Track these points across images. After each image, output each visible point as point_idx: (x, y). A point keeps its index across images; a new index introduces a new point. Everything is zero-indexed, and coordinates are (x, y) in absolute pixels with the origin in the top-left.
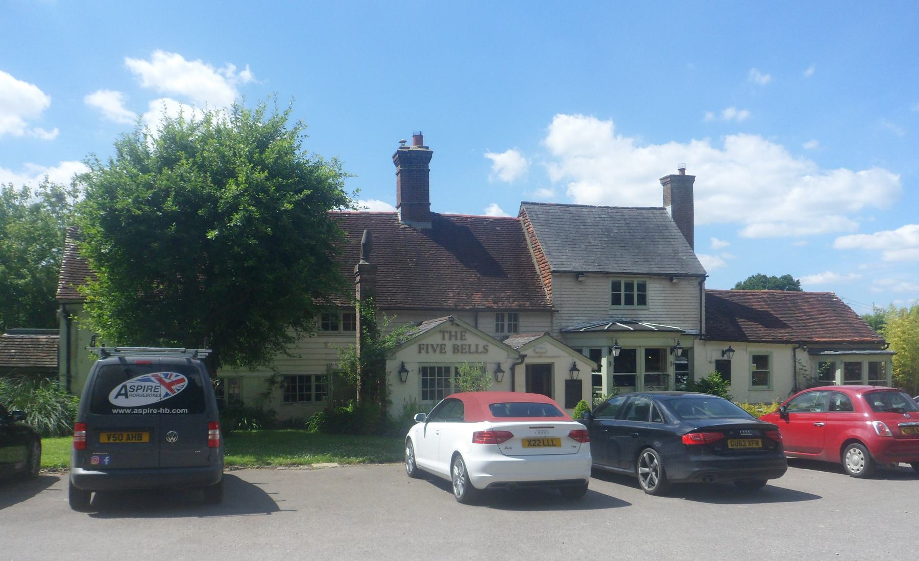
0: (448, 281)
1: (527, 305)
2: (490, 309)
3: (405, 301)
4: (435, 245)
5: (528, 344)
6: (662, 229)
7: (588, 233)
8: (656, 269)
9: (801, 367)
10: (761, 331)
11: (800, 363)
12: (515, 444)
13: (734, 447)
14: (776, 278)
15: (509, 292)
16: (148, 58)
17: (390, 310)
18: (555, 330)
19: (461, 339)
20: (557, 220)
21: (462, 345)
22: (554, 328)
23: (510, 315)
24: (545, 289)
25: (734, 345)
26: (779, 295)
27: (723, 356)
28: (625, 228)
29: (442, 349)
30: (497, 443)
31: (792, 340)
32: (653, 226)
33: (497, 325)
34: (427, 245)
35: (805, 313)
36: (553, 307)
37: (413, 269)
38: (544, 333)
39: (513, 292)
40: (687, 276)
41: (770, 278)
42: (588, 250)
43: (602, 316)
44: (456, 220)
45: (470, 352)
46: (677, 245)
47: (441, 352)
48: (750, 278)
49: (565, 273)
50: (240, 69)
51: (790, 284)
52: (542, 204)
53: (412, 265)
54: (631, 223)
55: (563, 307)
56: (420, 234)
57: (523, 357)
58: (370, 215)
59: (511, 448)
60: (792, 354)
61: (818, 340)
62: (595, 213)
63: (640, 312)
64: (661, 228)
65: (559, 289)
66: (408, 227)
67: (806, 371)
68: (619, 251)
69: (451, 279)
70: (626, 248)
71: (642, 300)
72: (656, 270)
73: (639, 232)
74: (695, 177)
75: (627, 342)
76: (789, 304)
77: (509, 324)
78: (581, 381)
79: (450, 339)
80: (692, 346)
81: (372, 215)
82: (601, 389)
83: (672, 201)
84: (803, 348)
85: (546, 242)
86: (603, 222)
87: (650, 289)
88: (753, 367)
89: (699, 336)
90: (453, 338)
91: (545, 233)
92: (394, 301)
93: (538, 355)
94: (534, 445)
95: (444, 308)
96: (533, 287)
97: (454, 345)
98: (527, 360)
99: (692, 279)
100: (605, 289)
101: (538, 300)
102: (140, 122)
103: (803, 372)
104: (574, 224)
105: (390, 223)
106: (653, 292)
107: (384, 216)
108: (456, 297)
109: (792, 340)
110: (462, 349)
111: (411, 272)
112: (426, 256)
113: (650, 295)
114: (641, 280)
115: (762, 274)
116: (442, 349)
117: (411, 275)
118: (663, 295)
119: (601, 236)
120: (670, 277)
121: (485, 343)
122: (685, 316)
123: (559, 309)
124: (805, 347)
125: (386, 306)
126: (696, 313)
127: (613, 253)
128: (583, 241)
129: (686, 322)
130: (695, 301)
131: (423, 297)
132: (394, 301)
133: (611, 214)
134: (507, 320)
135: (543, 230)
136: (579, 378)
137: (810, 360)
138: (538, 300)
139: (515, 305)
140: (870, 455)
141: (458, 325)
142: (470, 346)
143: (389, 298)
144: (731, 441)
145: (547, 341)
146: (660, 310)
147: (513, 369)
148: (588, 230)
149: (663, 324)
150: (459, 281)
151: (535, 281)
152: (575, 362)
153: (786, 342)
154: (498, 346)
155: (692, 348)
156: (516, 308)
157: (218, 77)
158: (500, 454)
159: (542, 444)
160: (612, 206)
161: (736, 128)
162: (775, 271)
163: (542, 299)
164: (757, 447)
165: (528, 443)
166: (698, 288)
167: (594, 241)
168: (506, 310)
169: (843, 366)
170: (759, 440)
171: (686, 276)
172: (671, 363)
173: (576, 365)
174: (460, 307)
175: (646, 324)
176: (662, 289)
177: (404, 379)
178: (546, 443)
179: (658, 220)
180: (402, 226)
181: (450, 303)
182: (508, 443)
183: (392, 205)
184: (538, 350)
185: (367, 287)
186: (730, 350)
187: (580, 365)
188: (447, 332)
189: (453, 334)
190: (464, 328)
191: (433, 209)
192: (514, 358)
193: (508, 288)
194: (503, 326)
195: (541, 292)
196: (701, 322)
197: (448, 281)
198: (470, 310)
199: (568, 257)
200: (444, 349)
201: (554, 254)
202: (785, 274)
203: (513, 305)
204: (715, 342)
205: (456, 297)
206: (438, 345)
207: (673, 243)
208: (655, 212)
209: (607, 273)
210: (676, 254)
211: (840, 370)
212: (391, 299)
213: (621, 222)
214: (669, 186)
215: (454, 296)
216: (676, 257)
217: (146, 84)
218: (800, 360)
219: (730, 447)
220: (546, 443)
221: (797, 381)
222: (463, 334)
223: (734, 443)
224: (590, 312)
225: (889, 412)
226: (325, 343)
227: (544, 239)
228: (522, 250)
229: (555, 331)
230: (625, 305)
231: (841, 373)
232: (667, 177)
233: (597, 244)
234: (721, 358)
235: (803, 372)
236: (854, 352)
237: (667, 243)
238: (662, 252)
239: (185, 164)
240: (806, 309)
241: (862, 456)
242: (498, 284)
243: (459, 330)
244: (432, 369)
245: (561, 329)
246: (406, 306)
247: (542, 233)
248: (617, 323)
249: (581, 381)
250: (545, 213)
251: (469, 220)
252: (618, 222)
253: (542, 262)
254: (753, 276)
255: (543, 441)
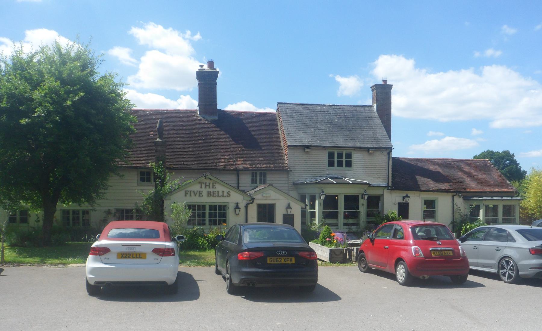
0: (223, 152)
1: (271, 167)
2: (246, 169)
3: (192, 164)
4: (218, 130)
5: (259, 191)
6: (368, 119)
7: (318, 122)
8: (359, 144)
9: (457, 208)
10: (432, 184)
11: (456, 205)
12: (112, 256)
13: (272, 263)
14: (499, 152)
15: (261, 159)
16: (141, 27)
17: (170, 169)
18: (290, 183)
19: (213, 188)
20: (299, 113)
21: (213, 192)
22: (289, 181)
23: (261, 174)
24: (285, 157)
25: (410, 194)
26: (449, 161)
27: (403, 200)
28: (344, 118)
29: (200, 194)
30: (100, 255)
31: (451, 190)
32: (362, 117)
33: (252, 180)
34: (213, 130)
35: (465, 173)
36: (289, 168)
37: (202, 144)
38: (268, 184)
39: (264, 159)
40: (379, 149)
41: (496, 152)
42: (315, 132)
43: (321, 174)
44: (235, 114)
45: (218, 196)
46: (376, 129)
47: (199, 196)
48: (483, 152)
49: (296, 146)
50: (193, 34)
51: (508, 156)
52: (291, 104)
53: (201, 142)
54: (348, 115)
55: (295, 168)
56: (210, 123)
57: (253, 199)
58: (180, 112)
59: (157, 259)
60: (452, 199)
61: (469, 190)
62: (325, 109)
63: (347, 172)
64: (368, 118)
65: (293, 157)
66: (203, 118)
67: (460, 210)
68: (336, 133)
69: (225, 151)
70: (341, 131)
71: (349, 164)
72: (358, 145)
73: (352, 121)
74: (392, 85)
75: (331, 191)
76: (456, 167)
77: (260, 179)
78: (293, 215)
79: (206, 188)
80: (382, 194)
81: (181, 112)
82: (315, 220)
83: (376, 101)
84: (459, 195)
85: (288, 127)
86: (330, 114)
87: (354, 157)
88: (425, 208)
89: (387, 187)
90: (207, 187)
91: (289, 122)
92: (186, 164)
93: (265, 198)
94: (125, 257)
95: (217, 169)
96: (277, 156)
97: (208, 192)
98: (256, 202)
99: (382, 151)
100: (324, 157)
101: (279, 164)
102: (3, 54)
103: (459, 211)
104: (310, 116)
105: (192, 116)
106: (356, 159)
107: (189, 112)
108: (226, 162)
109: (451, 190)
110: (213, 194)
111: (200, 146)
112: (211, 136)
113: (354, 162)
114: (348, 151)
115: (491, 150)
116: (200, 194)
117: (199, 148)
118: (363, 161)
119: (326, 123)
120: (368, 149)
121: (228, 190)
122: (378, 174)
123: (293, 169)
124: (460, 195)
125: (180, 167)
126: (385, 172)
127: (331, 134)
128: (313, 127)
129: (378, 178)
130: (385, 165)
131: (205, 162)
132: (186, 164)
133: (336, 109)
134: (259, 176)
135: (288, 120)
136: (292, 213)
137: (464, 203)
138: (279, 164)
139: (263, 167)
140: (408, 270)
141: (211, 179)
142: (218, 192)
143: (182, 162)
144: (270, 259)
145: (271, 190)
146: (360, 170)
147: (246, 207)
148: (318, 120)
149: (357, 179)
150: (230, 152)
151: (279, 152)
152: (289, 203)
153: (447, 192)
154: (237, 192)
155: (383, 195)
156: (265, 168)
157: (181, 38)
158: (100, 262)
159: (131, 256)
160: (337, 105)
161: (491, 62)
162: (499, 148)
163: (282, 163)
164: (291, 262)
165: (121, 256)
166: (387, 156)
167: (320, 127)
168: (257, 170)
169: (484, 207)
170: (292, 258)
171: (379, 149)
172: (362, 204)
173: (290, 205)
174: (227, 168)
175: (348, 180)
176: (362, 157)
177: (237, 213)
178: (135, 256)
179: (367, 113)
180: (199, 118)
181: (222, 165)
182: (107, 255)
183: (274, 109)
184: (264, 195)
185: (160, 155)
186: (407, 196)
187: (293, 205)
188: (204, 183)
189: (208, 184)
190: (215, 181)
191: (218, 107)
192: (248, 200)
193: (261, 156)
194: (256, 180)
195: (283, 159)
196: (388, 178)
197: (223, 152)
198: (233, 169)
199: (301, 137)
200: (202, 194)
201: (292, 135)
202: (505, 150)
203: (262, 167)
204: (398, 191)
205: (226, 162)
206: (197, 191)
207: (374, 128)
208: (365, 108)
209: (325, 147)
210: (375, 135)
211: (482, 210)
212: (184, 163)
213: (341, 115)
214: (375, 91)
215: (225, 161)
216: (375, 137)
217: (142, 42)
218: (456, 203)
219: (269, 262)
220: (135, 256)
221: (454, 217)
222: (214, 184)
223: (272, 260)
224: (313, 172)
225: (425, 240)
226: (142, 190)
227: (288, 125)
228: (274, 133)
229: (289, 183)
230: (337, 167)
231: (483, 211)
232: (373, 86)
233: (323, 129)
234: (402, 201)
235: (459, 211)
236: (484, 198)
237: (370, 128)
238: (365, 133)
239: (14, 79)
240: (467, 170)
241: (404, 270)
242: (255, 154)
243: (211, 182)
244: (215, 206)
245: (294, 182)
246: (193, 167)
247: (287, 122)
248: (329, 179)
249: (293, 215)
250: (291, 110)
251: (243, 114)
252: (339, 115)
253: (285, 140)
254: (484, 151)
255: (133, 255)
